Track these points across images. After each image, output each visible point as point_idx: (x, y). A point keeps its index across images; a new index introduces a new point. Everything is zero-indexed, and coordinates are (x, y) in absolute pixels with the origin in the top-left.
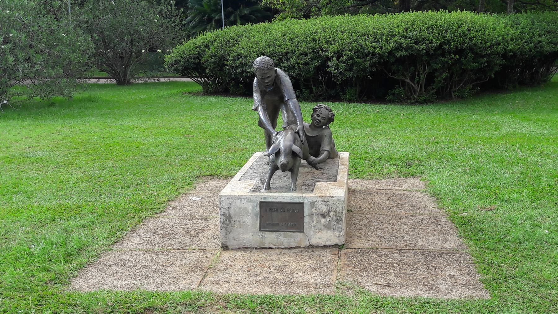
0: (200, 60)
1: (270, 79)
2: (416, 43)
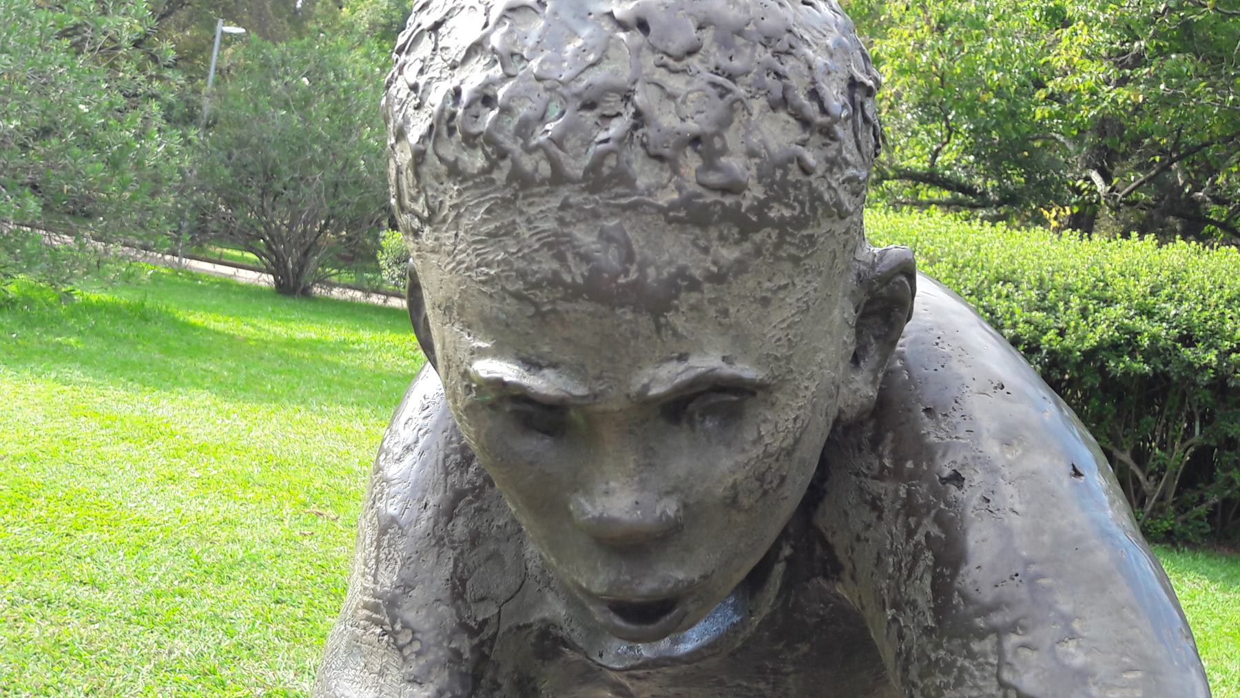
1: (717, 464)
2: (1188, 340)
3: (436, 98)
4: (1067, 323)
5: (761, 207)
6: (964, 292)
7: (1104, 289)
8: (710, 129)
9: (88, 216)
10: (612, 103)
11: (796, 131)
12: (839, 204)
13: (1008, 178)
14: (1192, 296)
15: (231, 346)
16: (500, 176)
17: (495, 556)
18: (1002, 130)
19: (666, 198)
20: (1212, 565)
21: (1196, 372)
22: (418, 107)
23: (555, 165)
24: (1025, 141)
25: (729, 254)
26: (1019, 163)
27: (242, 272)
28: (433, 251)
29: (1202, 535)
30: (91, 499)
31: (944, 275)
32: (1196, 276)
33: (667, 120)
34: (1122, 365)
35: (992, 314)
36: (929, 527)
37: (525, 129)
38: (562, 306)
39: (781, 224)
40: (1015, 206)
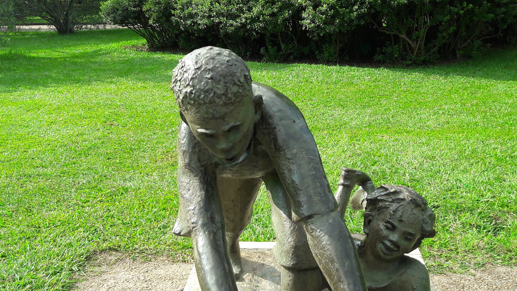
0: (142, 8)
1: (236, 137)
5: (235, 100)
10: (210, 91)
11: (237, 87)
23: (204, 101)
25: (232, 108)
27: (42, 27)
34: (396, 2)
36: (272, 136)
39: (239, 102)
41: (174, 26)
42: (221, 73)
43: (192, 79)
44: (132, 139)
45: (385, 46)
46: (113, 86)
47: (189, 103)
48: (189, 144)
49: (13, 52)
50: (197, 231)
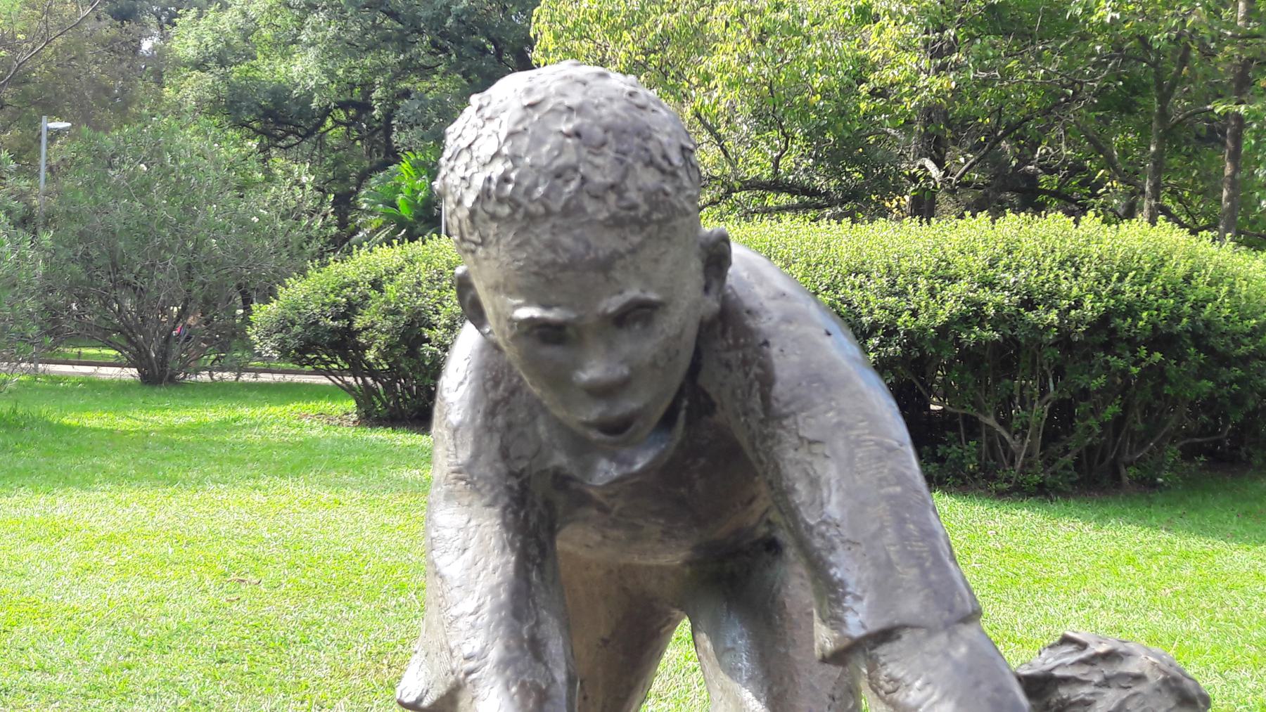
0: (351, 322)
1: (642, 346)
3: (478, 182)
4: (918, 303)
5: (648, 215)
6: (821, 288)
7: (947, 268)
8: (618, 180)
9: (1131, 112)
10: (569, 174)
12: (685, 209)
13: (848, 175)
14: (1027, 263)
15: (111, 441)
16: (519, 216)
17: (522, 435)
18: (835, 131)
19: (603, 215)
20: (1083, 509)
21: (1041, 332)
22: (468, 188)
24: (859, 137)
25: (636, 239)
26: (855, 161)
27: (104, 370)
28: (486, 259)
29: (1072, 483)
30: (16, 598)
31: (800, 274)
32: (1028, 244)
33: (597, 178)
34: (973, 336)
35: (849, 305)
36: (756, 370)
37: (528, 192)
38: (559, 275)
39: (659, 222)
40: (858, 202)
41: (427, 368)
42: (608, 120)
43: (511, 135)
44: (289, 618)
45: (943, 443)
46: (258, 497)
47: (493, 217)
48: (474, 403)
49: (20, 411)
50: (483, 683)
